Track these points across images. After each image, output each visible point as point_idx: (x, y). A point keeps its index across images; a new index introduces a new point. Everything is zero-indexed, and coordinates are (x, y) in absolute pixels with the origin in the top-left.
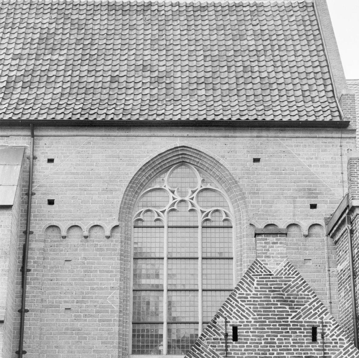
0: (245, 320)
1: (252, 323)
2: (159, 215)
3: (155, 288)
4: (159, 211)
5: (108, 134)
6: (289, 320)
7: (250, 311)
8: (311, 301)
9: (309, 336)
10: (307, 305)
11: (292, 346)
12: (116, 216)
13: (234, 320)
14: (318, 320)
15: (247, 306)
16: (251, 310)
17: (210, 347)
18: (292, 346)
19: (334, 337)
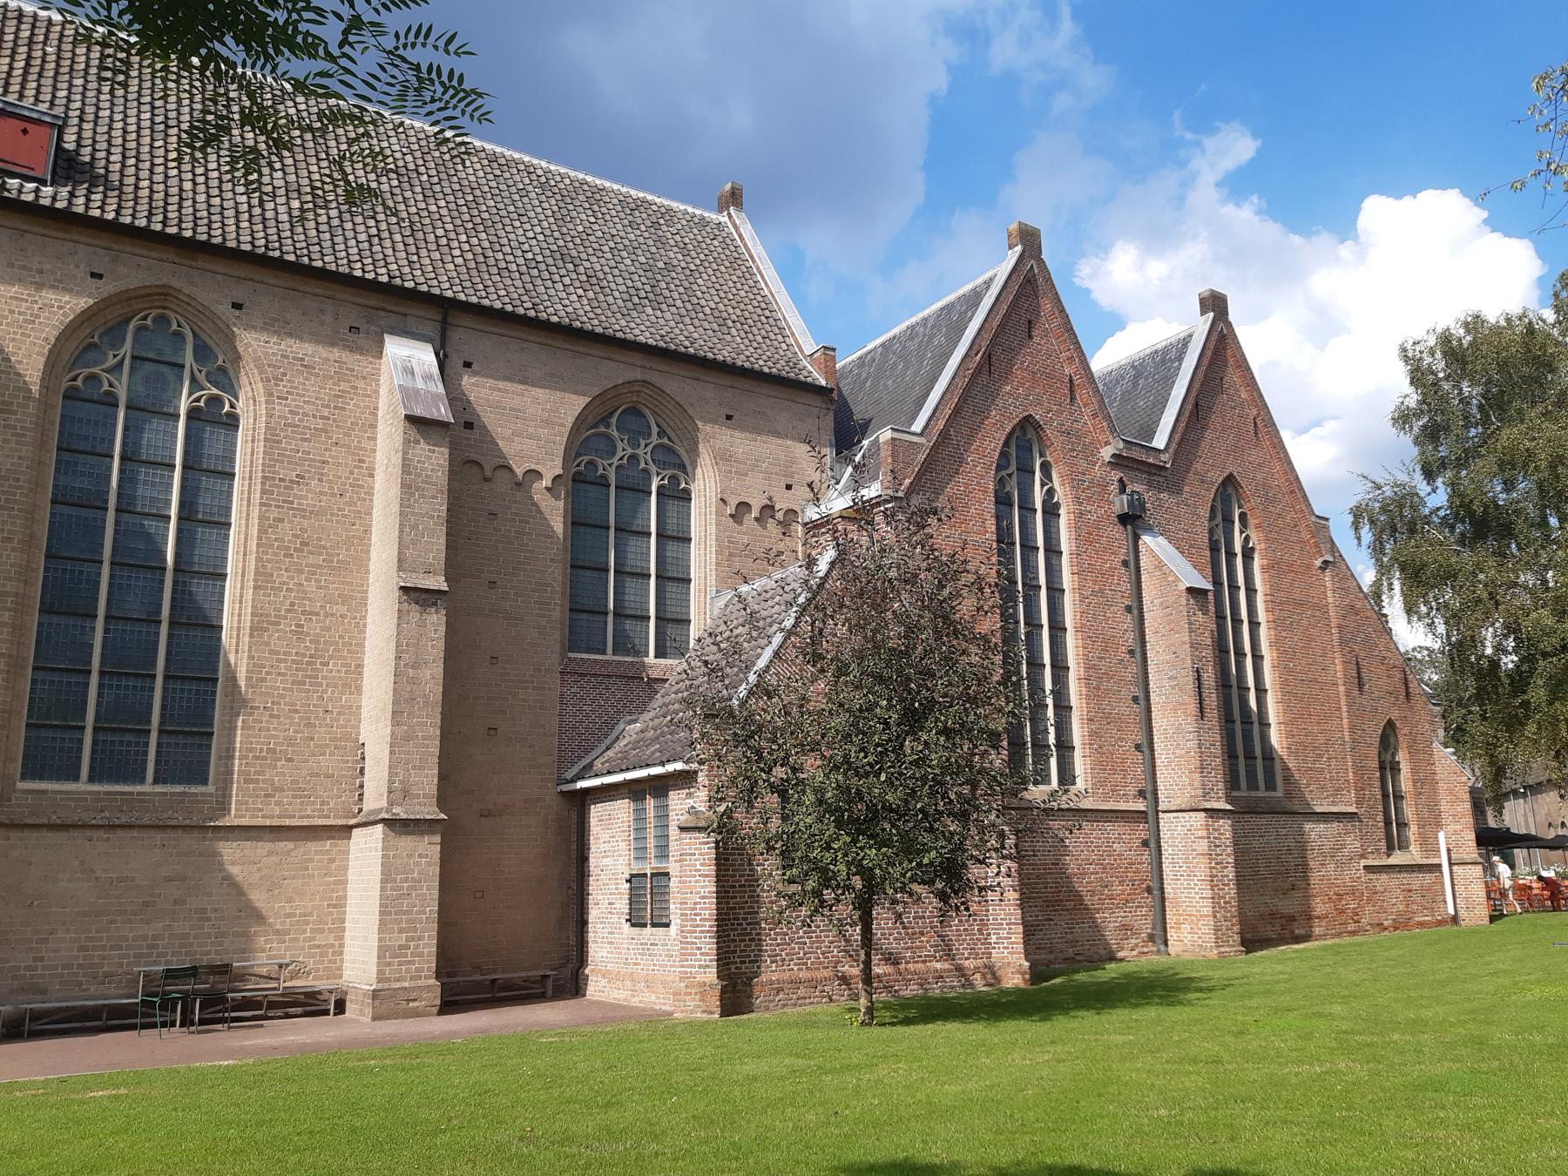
3: (1126, 815)
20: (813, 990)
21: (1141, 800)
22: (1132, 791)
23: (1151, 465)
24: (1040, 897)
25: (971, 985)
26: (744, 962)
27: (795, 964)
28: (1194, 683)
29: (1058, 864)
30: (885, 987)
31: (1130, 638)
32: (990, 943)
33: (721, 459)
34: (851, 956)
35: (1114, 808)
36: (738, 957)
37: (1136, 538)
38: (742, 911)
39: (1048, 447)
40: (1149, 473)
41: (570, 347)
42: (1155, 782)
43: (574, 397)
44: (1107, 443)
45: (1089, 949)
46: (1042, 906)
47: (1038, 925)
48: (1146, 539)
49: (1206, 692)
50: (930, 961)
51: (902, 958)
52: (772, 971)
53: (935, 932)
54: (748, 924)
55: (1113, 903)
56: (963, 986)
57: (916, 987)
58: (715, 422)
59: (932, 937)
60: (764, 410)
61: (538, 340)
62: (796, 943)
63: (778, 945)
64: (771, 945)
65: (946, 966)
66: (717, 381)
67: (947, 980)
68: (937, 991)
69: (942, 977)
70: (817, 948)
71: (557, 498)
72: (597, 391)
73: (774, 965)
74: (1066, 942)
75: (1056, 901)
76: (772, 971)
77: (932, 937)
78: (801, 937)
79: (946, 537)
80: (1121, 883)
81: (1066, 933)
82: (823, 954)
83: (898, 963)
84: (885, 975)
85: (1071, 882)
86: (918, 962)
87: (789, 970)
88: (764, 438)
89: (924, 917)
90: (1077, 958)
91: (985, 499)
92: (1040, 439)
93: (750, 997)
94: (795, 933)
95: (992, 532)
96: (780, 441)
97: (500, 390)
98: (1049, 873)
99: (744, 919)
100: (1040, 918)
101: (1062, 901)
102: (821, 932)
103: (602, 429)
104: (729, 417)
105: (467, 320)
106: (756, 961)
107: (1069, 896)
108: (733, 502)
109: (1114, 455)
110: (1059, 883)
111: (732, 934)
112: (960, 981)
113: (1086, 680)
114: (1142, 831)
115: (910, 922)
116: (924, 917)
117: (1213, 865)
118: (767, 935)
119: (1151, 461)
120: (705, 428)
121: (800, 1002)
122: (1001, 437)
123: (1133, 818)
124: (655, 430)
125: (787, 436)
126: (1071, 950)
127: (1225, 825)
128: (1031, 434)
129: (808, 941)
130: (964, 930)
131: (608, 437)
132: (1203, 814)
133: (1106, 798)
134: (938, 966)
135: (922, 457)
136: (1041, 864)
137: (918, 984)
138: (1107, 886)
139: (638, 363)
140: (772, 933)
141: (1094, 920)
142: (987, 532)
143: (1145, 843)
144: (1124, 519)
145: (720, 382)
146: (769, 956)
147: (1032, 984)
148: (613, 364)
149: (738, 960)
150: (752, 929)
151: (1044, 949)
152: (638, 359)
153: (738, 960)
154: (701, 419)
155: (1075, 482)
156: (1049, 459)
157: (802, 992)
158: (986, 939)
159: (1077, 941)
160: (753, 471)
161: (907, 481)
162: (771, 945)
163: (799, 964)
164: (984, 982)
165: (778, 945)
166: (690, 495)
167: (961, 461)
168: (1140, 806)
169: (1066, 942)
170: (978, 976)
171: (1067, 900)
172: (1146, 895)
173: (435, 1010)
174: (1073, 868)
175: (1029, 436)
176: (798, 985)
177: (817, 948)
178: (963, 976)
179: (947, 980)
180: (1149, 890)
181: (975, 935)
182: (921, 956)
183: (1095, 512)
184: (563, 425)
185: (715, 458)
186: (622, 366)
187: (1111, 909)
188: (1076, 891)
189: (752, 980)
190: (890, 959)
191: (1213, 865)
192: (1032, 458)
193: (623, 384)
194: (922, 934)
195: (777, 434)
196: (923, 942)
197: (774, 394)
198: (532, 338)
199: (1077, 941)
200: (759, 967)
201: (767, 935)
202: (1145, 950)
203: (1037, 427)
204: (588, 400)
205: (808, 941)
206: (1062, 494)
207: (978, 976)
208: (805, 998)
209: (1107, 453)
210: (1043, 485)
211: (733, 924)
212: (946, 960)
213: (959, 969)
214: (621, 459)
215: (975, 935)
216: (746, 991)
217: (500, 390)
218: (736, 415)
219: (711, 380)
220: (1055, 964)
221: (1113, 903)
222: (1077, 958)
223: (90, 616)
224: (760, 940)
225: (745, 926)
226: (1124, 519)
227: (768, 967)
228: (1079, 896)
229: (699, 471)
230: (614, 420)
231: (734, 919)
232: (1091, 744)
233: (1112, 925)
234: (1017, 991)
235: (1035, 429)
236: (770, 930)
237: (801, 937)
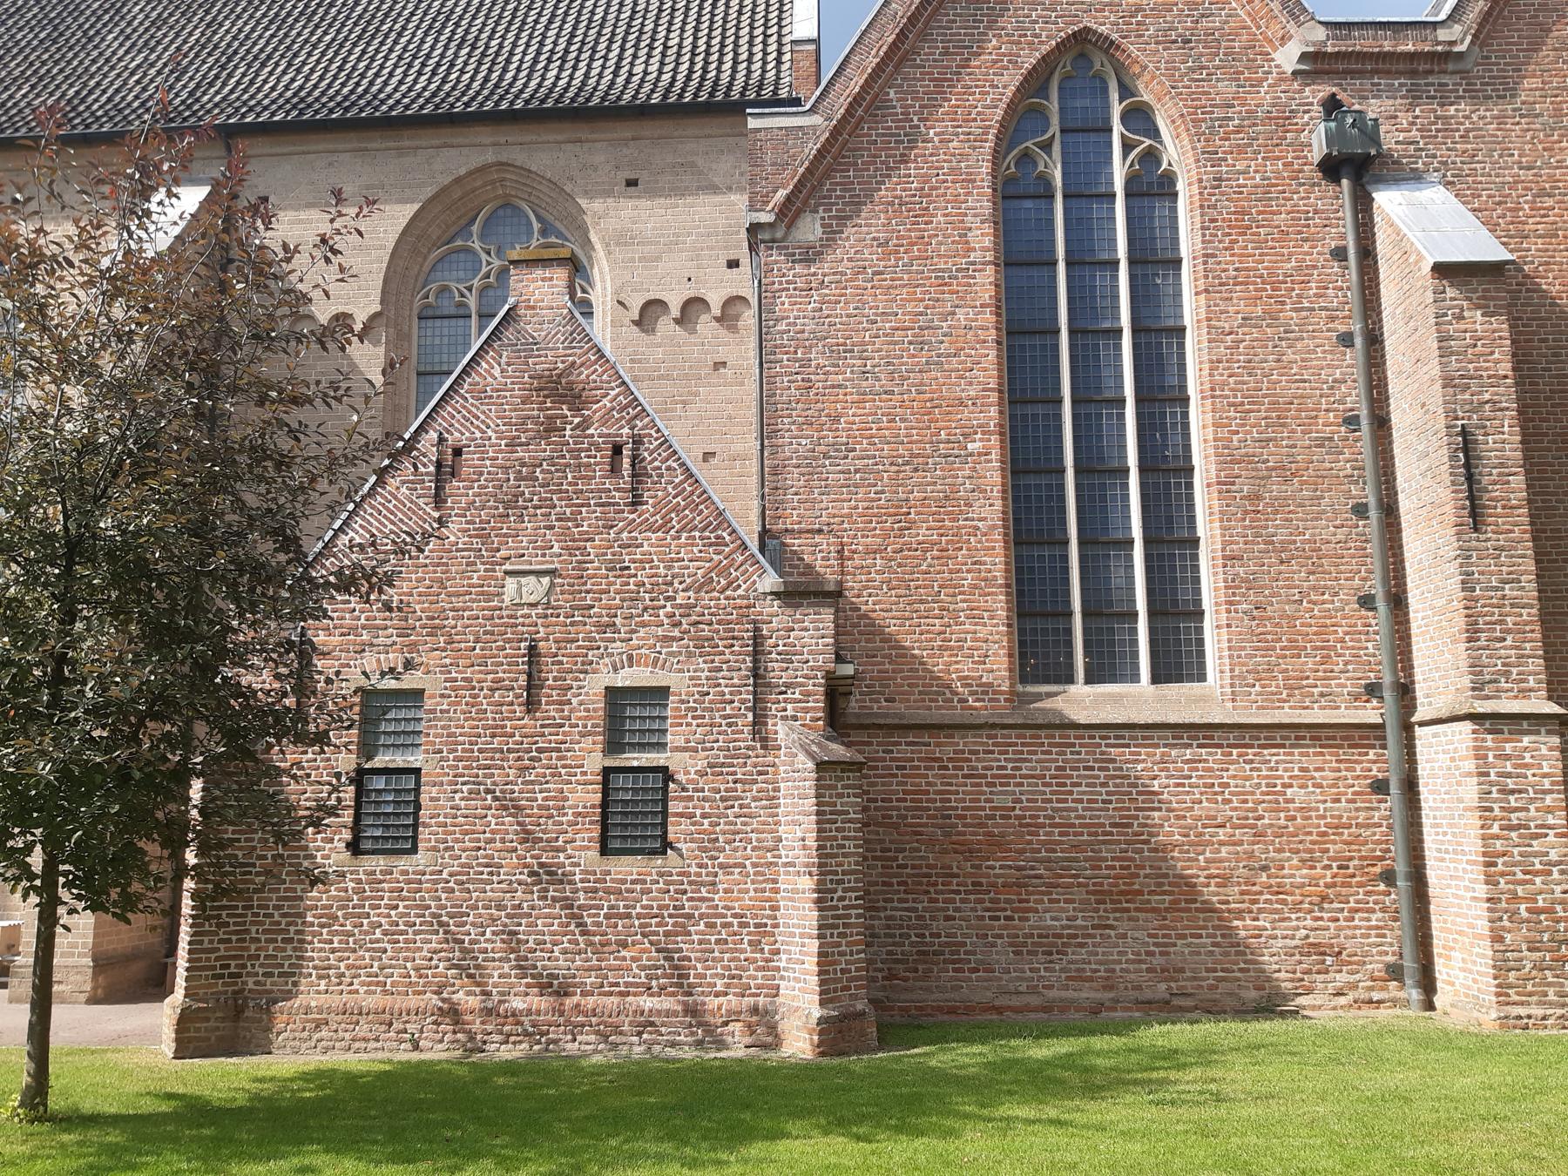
0: (478, 435)
1: (494, 441)
2: (463, 295)
3: (1323, 733)
4: (461, 287)
5: (304, 148)
6: (568, 433)
7: (488, 417)
8: (613, 393)
9: (1559, 792)
10: (605, 401)
11: (570, 484)
12: (376, 295)
13: (457, 434)
14: (626, 431)
15: (485, 408)
16: (492, 415)
17: (404, 490)
18: (570, 484)
19: (657, 464)
20: (384, 1028)
21: (1375, 702)
22: (1347, 685)
23: (1412, 56)
24: (1079, 885)
25: (721, 1044)
26: (270, 975)
27: (363, 984)
28: (1453, 458)
29: (1130, 825)
30: (526, 1034)
31: (1355, 398)
32: (778, 969)
33: (618, 244)
34: (470, 976)
35: (1297, 721)
36: (261, 965)
37: (1363, 206)
38: (274, 896)
39: (1139, 76)
40: (1413, 73)
41: (392, 144)
42: (1408, 667)
43: (398, 207)
44: (1284, 39)
45: (1211, 988)
46: (1087, 902)
47: (1076, 936)
48: (1387, 200)
49: (1488, 475)
50: (635, 995)
51: (575, 985)
52: (319, 992)
53: (651, 943)
54: (284, 915)
55: (1284, 902)
56: (699, 1044)
57: (592, 1038)
58: (608, 193)
59: (644, 951)
60: (690, 159)
61: (349, 146)
62: (368, 950)
63: (333, 951)
64: (321, 950)
65: (668, 1003)
66: (609, 136)
67: (663, 1030)
68: (637, 1049)
69: (652, 1024)
70: (406, 959)
71: (376, 343)
72: (429, 191)
73: (323, 982)
74: (1149, 970)
75: (1122, 893)
76: (319, 992)
77: (644, 951)
78: (378, 941)
79: (875, 273)
80: (1309, 863)
81: (1149, 953)
82: (417, 969)
83: (566, 994)
84: (529, 1012)
85: (1165, 859)
86: (611, 994)
87: (350, 992)
88: (689, 200)
89: (629, 916)
90: (1176, 1002)
91: (967, 194)
92: (1120, 69)
93: (269, 1030)
94: (367, 933)
95: (984, 249)
96: (718, 199)
97: (301, 222)
98: (1104, 842)
99: (276, 907)
100: (1079, 922)
101: (1140, 893)
102: (415, 933)
103: (459, 243)
104: (632, 183)
105: (260, 146)
106: (292, 974)
107: (1160, 885)
108: (636, 303)
109: (1304, 57)
110: (1132, 859)
111: (254, 929)
112: (692, 1034)
113: (1225, 485)
114: (1378, 762)
115: (599, 924)
116: (629, 916)
117: (1495, 829)
118: (314, 934)
119: (1410, 47)
120: (592, 207)
121: (357, 1045)
122: (1010, 81)
123: (1131, 738)
124: (536, 226)
125: (730, 189)
126: (1163, 986)
127: (1543, 749)
128: (1098, 60)
129: (389, 947)
130: (718, 942)
131: (469, 250)
132: (1468, 726)
133: (1272, 700)
134: (648, 1003)
135: (812, 148)
136: (1081, 825)
137: (597, 1033)
138: (1265, 868)
139: (488, 140)
140: (325, 931)
141: (1229, 932)
142: (974, 250)
143: (1380, 787)
144: (1331, 168)
145: (615, 135)
146: (315, 968)
147: (822, 1054)
148: (453, 152)
149: (261, 971)
150: (289, 924)
151: (1091, 979)
152: (484, 135)
153: (261, 971)
154: (588, 194)
155: (1200, 124)
156: (1146, 98)
157: (363, 1030)
158: (767, 960)
159: (1182, 970)
160: (671, 251)
161: (781, 194)
162: (321, 950)
163: (370, 984)
164: (748, 1040)
165: (333, 951)
166: (591, 306)
167: (914, 138)
168: (1370, 714)
169: (1149, 970)
170: (736, 1027)
171: (1151, 893)
172: (1382, 887)
173: (83, 997)
174: (1170, 832)
175: (1097, 66)
176: (355, 1018)
177: (406, 959)
178: (699, 1025)
179: (663, 1030)
180: (1389, 877)
181: (743, 951)
182: (617, 984)
183: (1251, 172)
184: (382, 247)
185: (608, 245)
186: (465, 151)
187: (1276, 911)
188: (1182, 877)
189: (275, 1002)
190: (551, 985)
191: (1495, 829)
192: (1107, 108)
193: (470, 173)
194: (624, 945)
195: (714, 189)
196: (624, 959)
197: (708, 131)
198: (341, 147)
199: (1182, 970)
200: (295, 984)
201: (314, 934)
202: (1376, 996)
203: (1108, 46)
204: (416, 206)
205: (389, 947)
206: (1176, 152)
207: (736, 1027)
208: (365, 1040)
209: (1288, 57)
210: (1127, 147)
211: (257, 915)
212: (673, 994)
213: (693, 1011)
214: (487, 276)
215: (743, 951)
216: (260, 1021)
217: (301, 222)
218: (643, 177)
219: (603, 136)
220: (1114, 1009)
221: (1284, 902)
222: (1176, 1002)
223: (1056, 615)
224: (302, 941)
225: (277, 918)
226: (1331, 168)
227: (312, 984)
228: (1187, 888)
229: (596, 270)
230: (475, 228)
231: (259, 907)
232: (1231, 603)
233: (1280, 942)
234: (800, 1071)
235: (1106, 51)
236: (322, 926)
237: (378, 941)
